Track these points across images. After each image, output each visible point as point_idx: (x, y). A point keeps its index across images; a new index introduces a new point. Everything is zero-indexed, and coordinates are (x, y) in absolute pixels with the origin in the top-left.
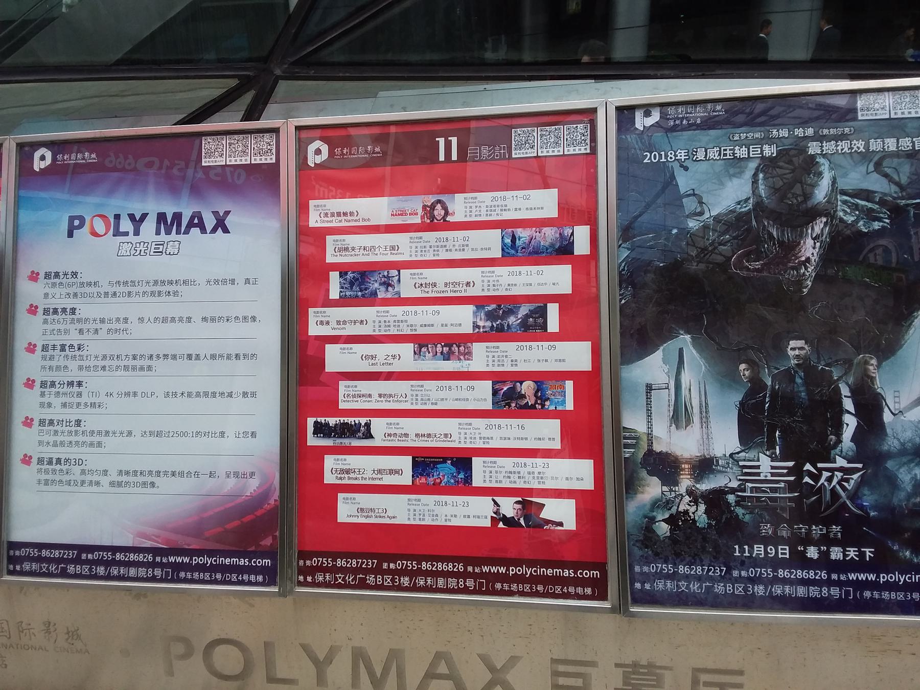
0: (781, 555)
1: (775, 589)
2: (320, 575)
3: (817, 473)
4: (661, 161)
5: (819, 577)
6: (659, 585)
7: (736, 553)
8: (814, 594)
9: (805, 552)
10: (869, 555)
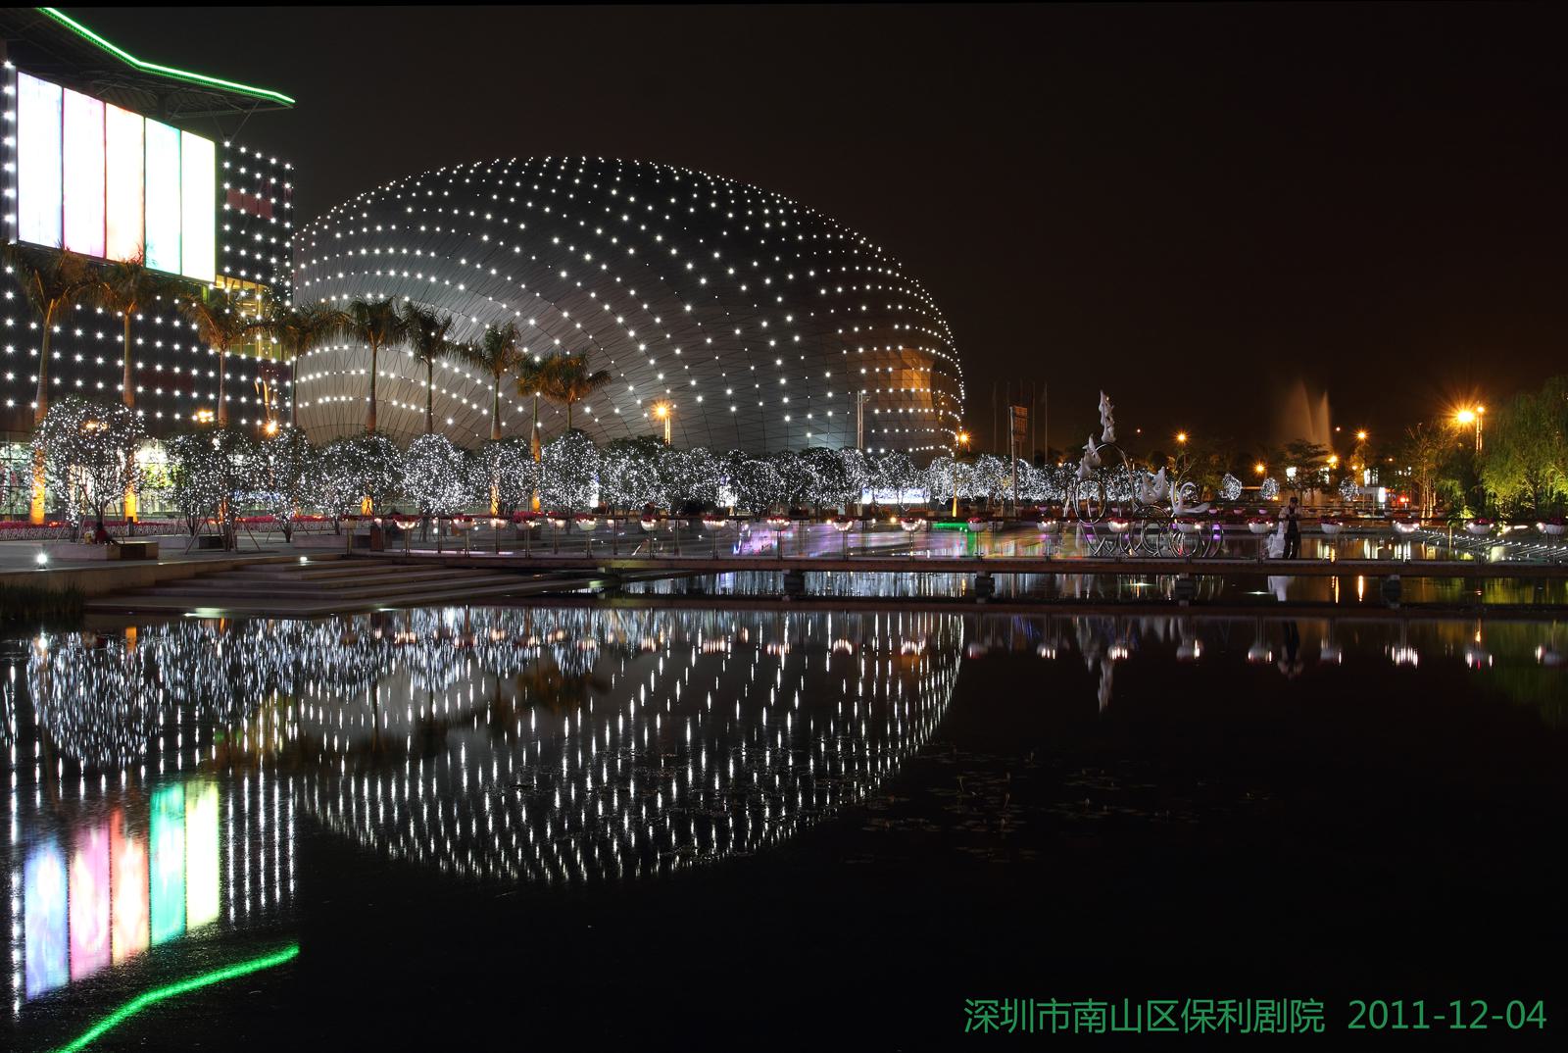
0: (1198, 1008)
1: (1191, 1013)
2: (1199, 1006)
4: (1394, 1027)
5: (1359, 1023)
6: (1270, 1018)
8: (1304, 1022)
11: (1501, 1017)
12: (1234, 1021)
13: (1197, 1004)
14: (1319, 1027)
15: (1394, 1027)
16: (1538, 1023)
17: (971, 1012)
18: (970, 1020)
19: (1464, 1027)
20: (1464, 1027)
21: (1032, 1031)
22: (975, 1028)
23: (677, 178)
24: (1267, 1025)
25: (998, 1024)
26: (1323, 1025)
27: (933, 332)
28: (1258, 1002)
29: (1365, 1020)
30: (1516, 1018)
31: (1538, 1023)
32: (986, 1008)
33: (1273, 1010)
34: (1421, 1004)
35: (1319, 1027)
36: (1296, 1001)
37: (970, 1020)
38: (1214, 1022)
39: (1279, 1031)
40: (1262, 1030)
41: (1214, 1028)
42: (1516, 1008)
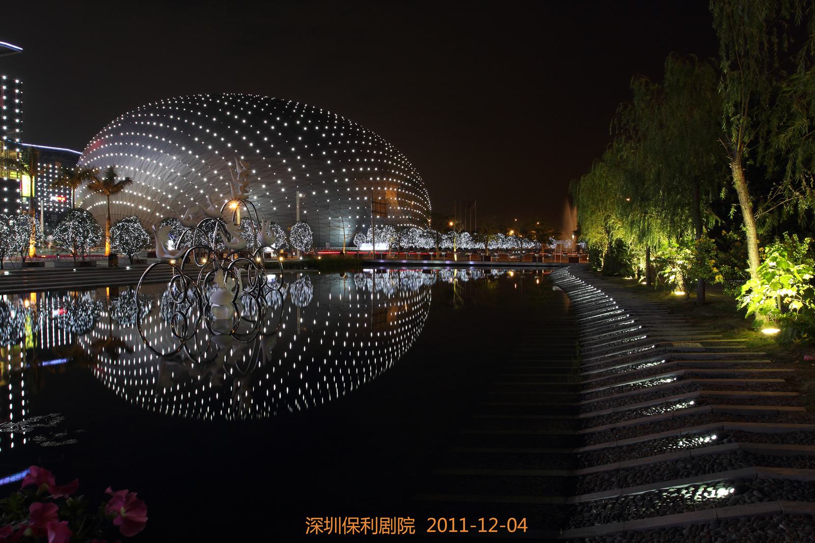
0: (351, 522)
1: (347, 524)
2: (351, 521)
3: (372, 299)
4: (450, 531)
6: (387, 527)
7: (462, 530)
8: (405, 529)
9: (20, 111)
10: (431, 530)
11: (505, 526)
12: (369, 528)
13: (350, 519)
14: (412, 531)
15: (450, 531)
16: (523, 529)
17: (309, 524)
18: (309, 528)
19: (486, 531)
20: (486, 531)
21: (340, 533)
22: (311, 532)
23: (321, 110)
24: (386, 530)
25: (323, 530)
26: (414, 530)
27: (412, 193)
28: (381, 519)
29: (435, 528)
30: (512, 527)
31: (523, 529)
32: (317, 522)
33: (389, 523)
34: (464, 519)
35: (412, 531)
36: (401, 518)
37: (309, 528)
38: (359, 529)
39: (392, 533)
40: (383, 533)
41: (359, 532)
42: (512, 522)
